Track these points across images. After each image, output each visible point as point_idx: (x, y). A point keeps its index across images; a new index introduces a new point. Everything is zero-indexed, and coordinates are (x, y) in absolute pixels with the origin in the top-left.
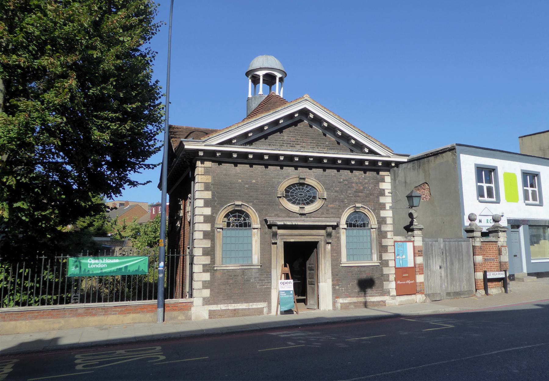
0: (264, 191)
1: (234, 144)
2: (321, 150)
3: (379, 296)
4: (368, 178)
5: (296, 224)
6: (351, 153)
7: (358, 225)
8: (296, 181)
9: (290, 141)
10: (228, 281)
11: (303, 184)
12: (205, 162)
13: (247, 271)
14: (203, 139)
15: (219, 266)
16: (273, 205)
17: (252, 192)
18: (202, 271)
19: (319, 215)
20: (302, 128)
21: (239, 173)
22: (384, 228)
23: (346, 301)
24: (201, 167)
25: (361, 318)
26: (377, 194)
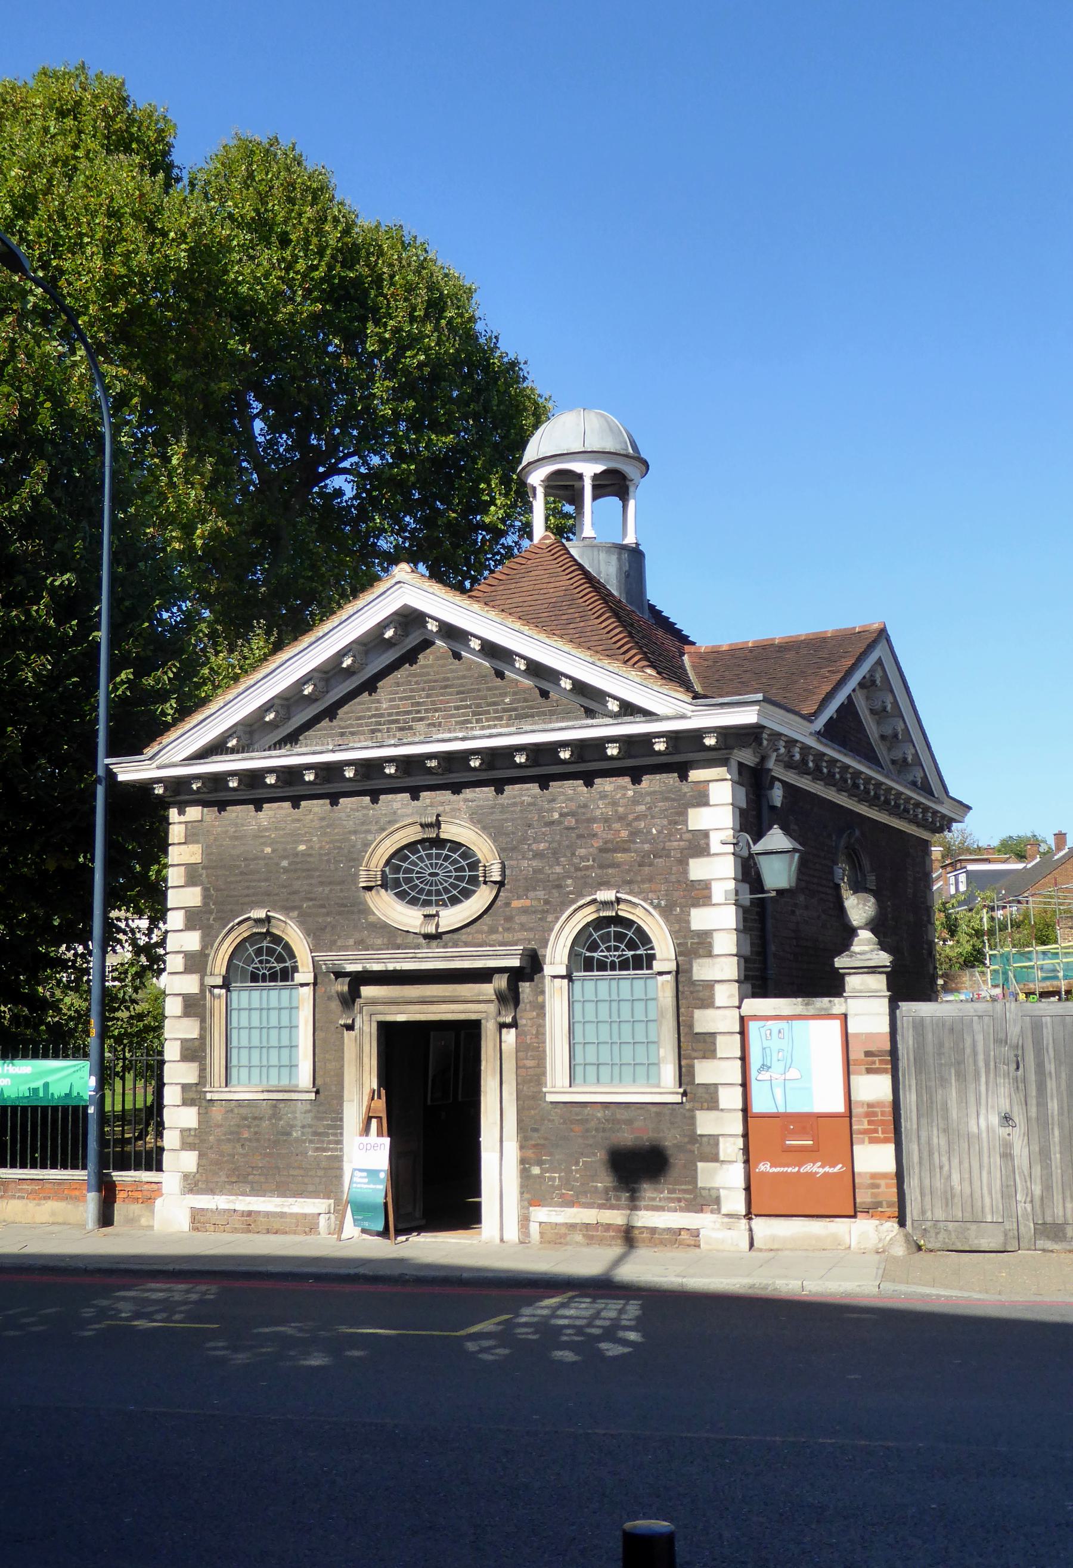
0: (328, 874)
1: (233, 751)
2: (489, 727)
3: (682, 1210)
4: (648, 799)
5: (398, 968)
6: (590, 722)
7: (613, 962)
8: (413, 834)
9: (398, 714)
10: (238, 1133)
11: (439, 843)
12: (187, 809)
13: (283, 1105)
14: (149, 751)
15: (216, 1092)
16: (353, 913)
17: (298, 878)
18: (179, 1103)
19: (480, 937)
20: (431, 666)
21: (266, 829)
22: (702, 970)
23: (560, 1219)
24: (180, 823)
25: (465, 1275)
26: (682, 850)
